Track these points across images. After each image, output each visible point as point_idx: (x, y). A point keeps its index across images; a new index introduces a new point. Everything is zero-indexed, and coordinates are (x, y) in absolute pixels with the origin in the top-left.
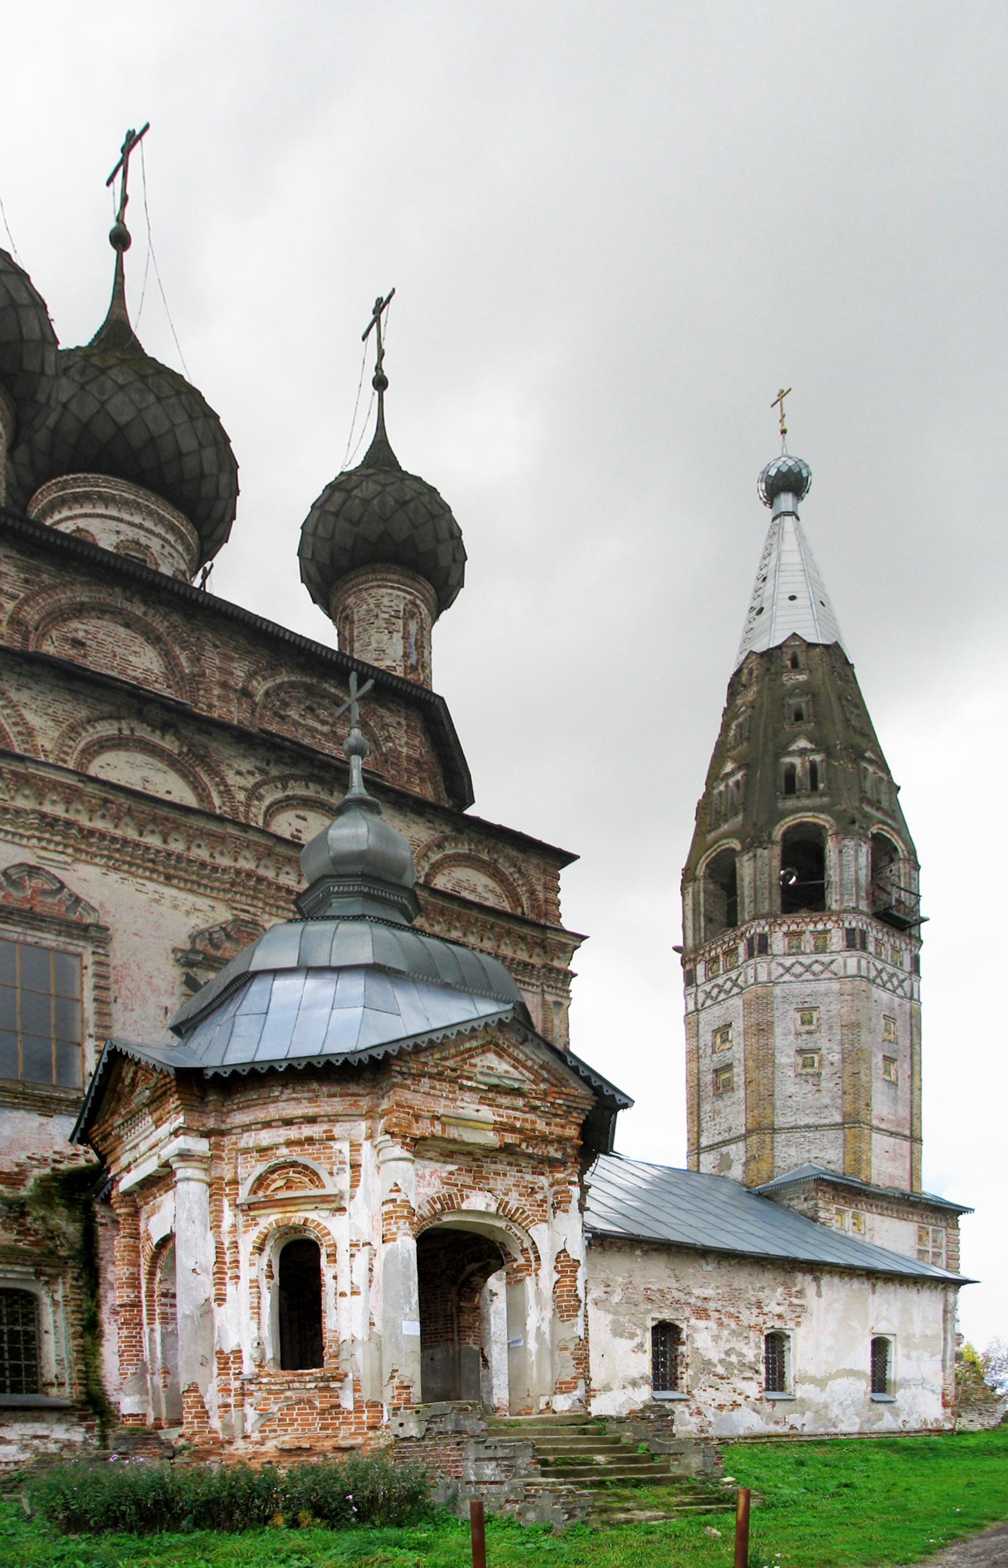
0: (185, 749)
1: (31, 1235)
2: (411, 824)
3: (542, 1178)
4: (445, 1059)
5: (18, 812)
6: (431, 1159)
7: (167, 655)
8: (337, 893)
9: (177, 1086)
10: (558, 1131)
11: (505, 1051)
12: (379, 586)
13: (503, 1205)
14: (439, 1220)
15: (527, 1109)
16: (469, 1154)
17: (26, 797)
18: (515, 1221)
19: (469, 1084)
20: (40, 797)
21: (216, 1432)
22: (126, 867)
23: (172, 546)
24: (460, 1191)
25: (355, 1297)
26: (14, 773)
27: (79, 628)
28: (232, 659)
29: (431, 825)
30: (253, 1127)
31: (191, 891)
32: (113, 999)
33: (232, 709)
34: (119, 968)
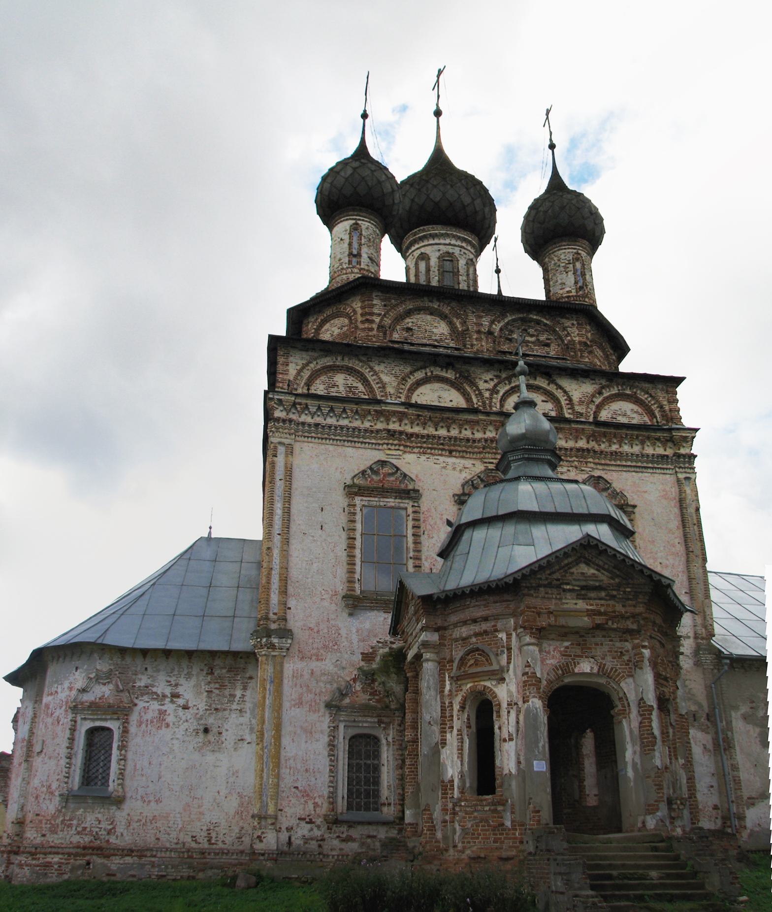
0: (458, 376)
1: (377, 695)
2: (581, 384)
3: (627, 644)
4: (553, 573)
5: (378, 431)
6: (553, 639)
7: (451, 324)
8: (513, 460)
9: (422, 605)
10: (631, 609)
11: (590, 561)
12: (559, 250)
13: (601, 667)
14: (562, 681)
15: (608, 598)
16: (577, 633)
17: (382, 422)
18: (611, 678)
19: (568, 587)
20: (388, 421)
21: (439, 842)
22: (429, 451)
23: (465, 249)
24: (573, 659)
25: (511, 742)
26: (376, 411)
27: (409, 322)
28: (482, 317)
29: (594, 382)
30: (458, 625)
31: (463, 457)
32: (422, 532)
33: (483, 344)
34: (426, 513)
